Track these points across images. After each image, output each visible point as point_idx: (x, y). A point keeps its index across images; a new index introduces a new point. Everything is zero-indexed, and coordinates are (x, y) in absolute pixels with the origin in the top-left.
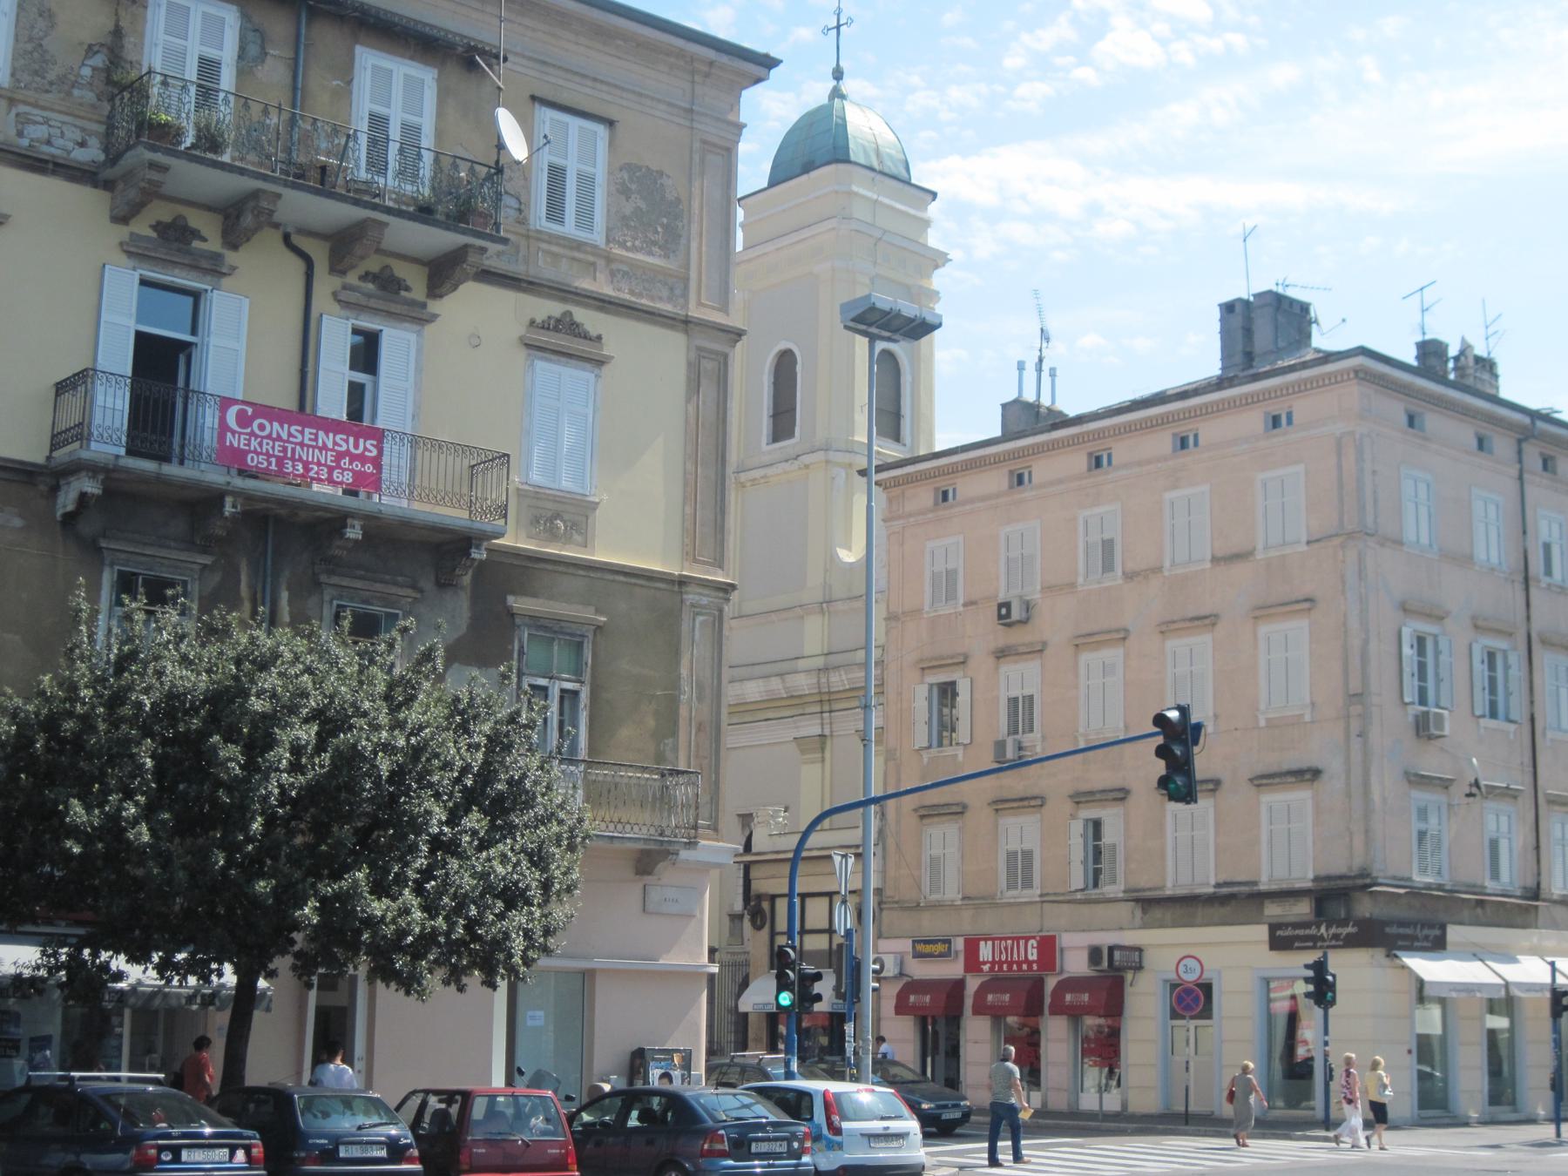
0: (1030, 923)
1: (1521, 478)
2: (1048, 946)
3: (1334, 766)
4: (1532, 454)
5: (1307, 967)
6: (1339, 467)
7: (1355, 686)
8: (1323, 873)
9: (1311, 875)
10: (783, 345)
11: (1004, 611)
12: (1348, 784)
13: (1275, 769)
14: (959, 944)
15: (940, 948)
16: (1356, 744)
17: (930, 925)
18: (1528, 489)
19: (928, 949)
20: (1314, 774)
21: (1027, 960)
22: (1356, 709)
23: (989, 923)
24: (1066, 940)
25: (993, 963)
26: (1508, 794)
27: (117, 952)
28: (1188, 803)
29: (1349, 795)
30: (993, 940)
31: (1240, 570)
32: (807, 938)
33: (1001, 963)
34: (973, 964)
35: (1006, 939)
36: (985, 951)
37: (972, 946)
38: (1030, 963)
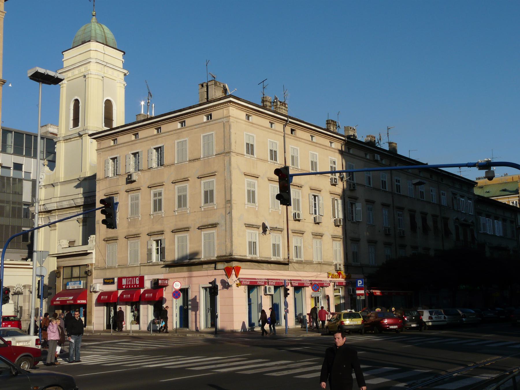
0: (136, 273)
1: (284, 137)
2: (142, 279)
3: (222, 222)
4: (288, 129)
5: (210, 283)
6: (224, 131)
7: (228, 198)
8: (219, 255)
9: (216, 256)
10: (76, 98)
11: (129, 177)
12: (226, 228)
13: (206, 224)
14: (116, 280)
15: (111, 281)
16: (228, 216)
17: (109, 274)
18: (286, 139)
19: (108, 281)
20: (214, 226)
21: (136, 284)
22: (229, 205)
23: (125, 273)
24: (146, 278)
25: (126, 285)
26: (281, 230)
27: (425, 322)
28: (113, 228)
29: (226, 231)
30: (126, 278)
31: (197, 164)
32: (242, 291)
33: (128, 285)
34: (120, 286)
35: (130, 277)
36: (124, 282)
37: (120, 280)
38: (137, 285)
